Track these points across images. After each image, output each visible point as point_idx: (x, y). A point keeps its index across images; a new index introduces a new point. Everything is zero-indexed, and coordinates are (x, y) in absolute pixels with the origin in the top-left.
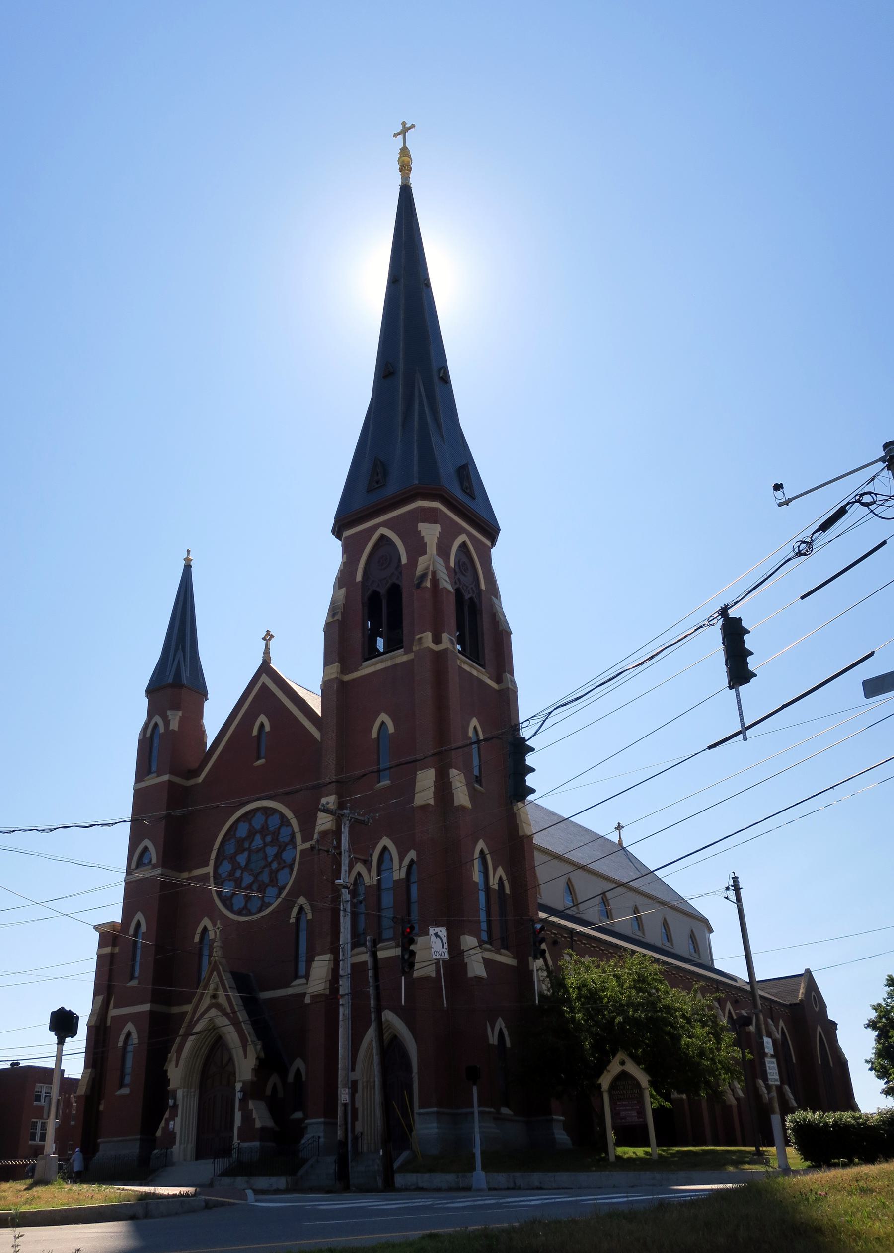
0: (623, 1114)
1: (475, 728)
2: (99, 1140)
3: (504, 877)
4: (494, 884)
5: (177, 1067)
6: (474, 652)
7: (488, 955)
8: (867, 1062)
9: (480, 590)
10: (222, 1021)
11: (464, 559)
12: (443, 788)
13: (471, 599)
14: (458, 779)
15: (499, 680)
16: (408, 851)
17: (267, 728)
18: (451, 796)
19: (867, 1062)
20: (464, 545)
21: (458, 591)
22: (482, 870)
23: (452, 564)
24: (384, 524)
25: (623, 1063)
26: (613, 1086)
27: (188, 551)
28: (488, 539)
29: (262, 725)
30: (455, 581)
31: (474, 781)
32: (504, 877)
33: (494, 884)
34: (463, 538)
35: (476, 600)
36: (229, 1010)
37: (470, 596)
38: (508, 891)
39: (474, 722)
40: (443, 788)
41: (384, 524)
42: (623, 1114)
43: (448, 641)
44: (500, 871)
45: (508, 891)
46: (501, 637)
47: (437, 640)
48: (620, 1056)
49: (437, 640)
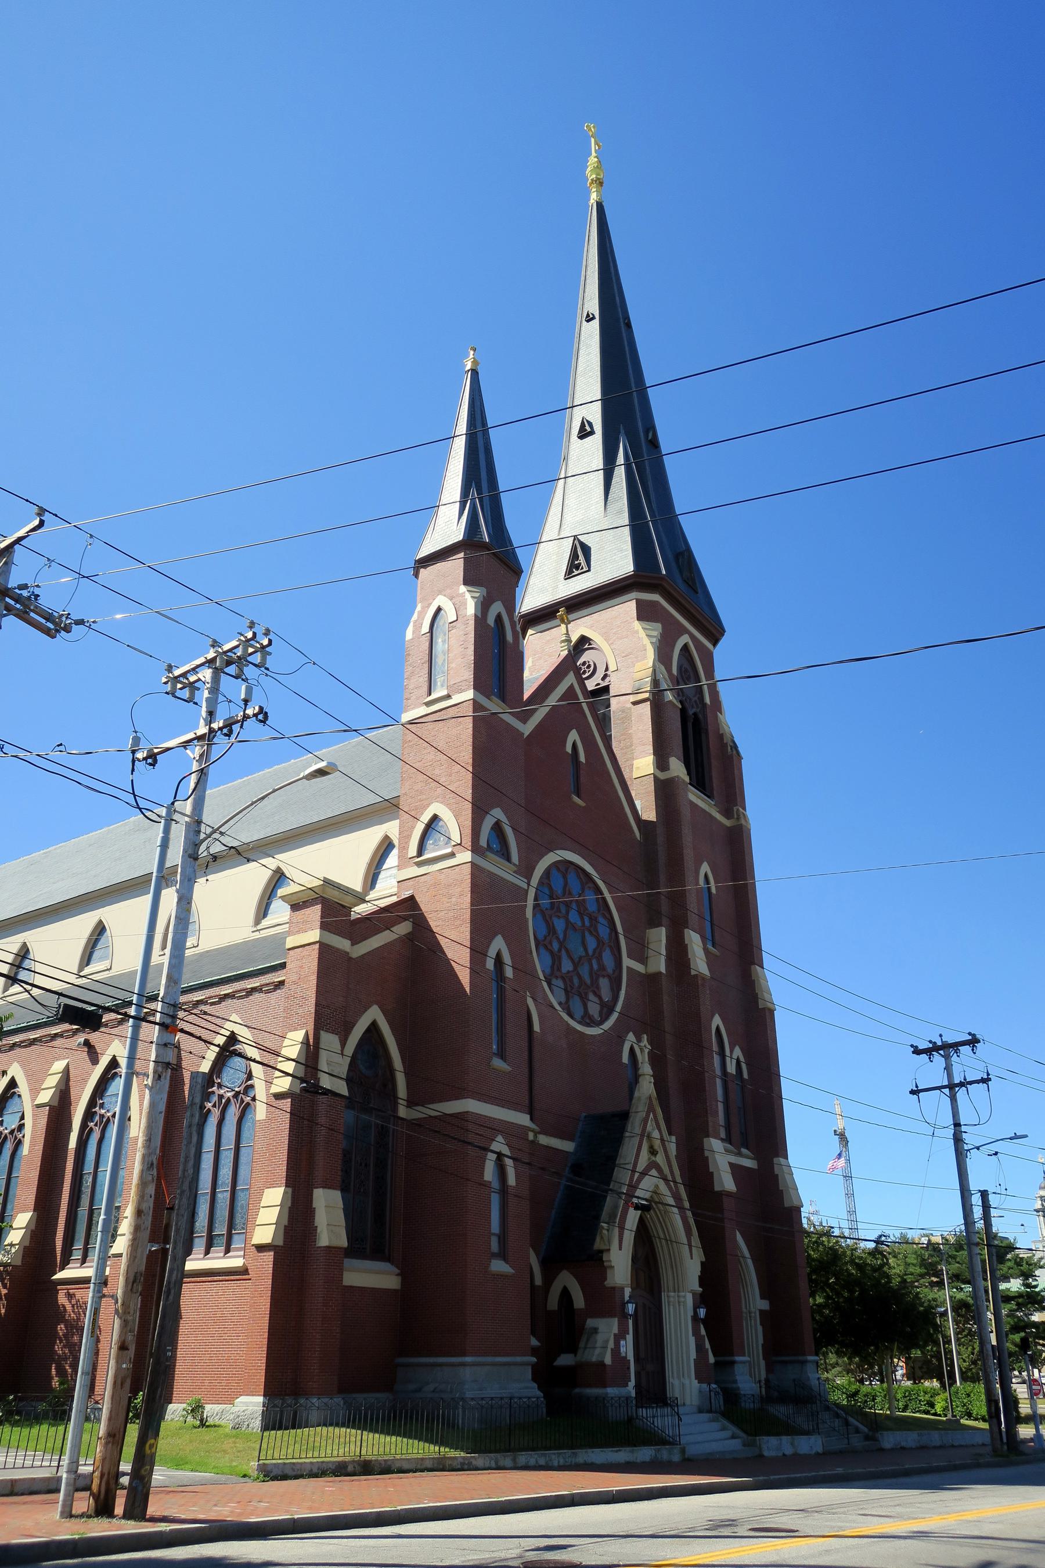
1: (706, 876)
3: (742, 1059)
4: (731, 1068)
5: (620, 1249)
6: (700, 781)
7: (734, 1159)
9: (704, 705)
10: (663, 1189)
11: (686, 665)
13: (695, 714)
14: (694, 941)
15: (728, 813)
20: (685, 648)
21: (683, 711)
22: (121, 1173)
23: (675, 671)
27: (973, 1041)
28: (710, 641)
30: (680, 694)
31: (711, 939)
32: (742, 1059)
33: (731, 1068)
34: (685, 639)
35: (700, 716)
36: (670, 1178)
37: (694, 710)
38: (746, 1076)
39: (705, 868)
44: (738, 1052)
45: (746, 1076)
46: (730, 758)
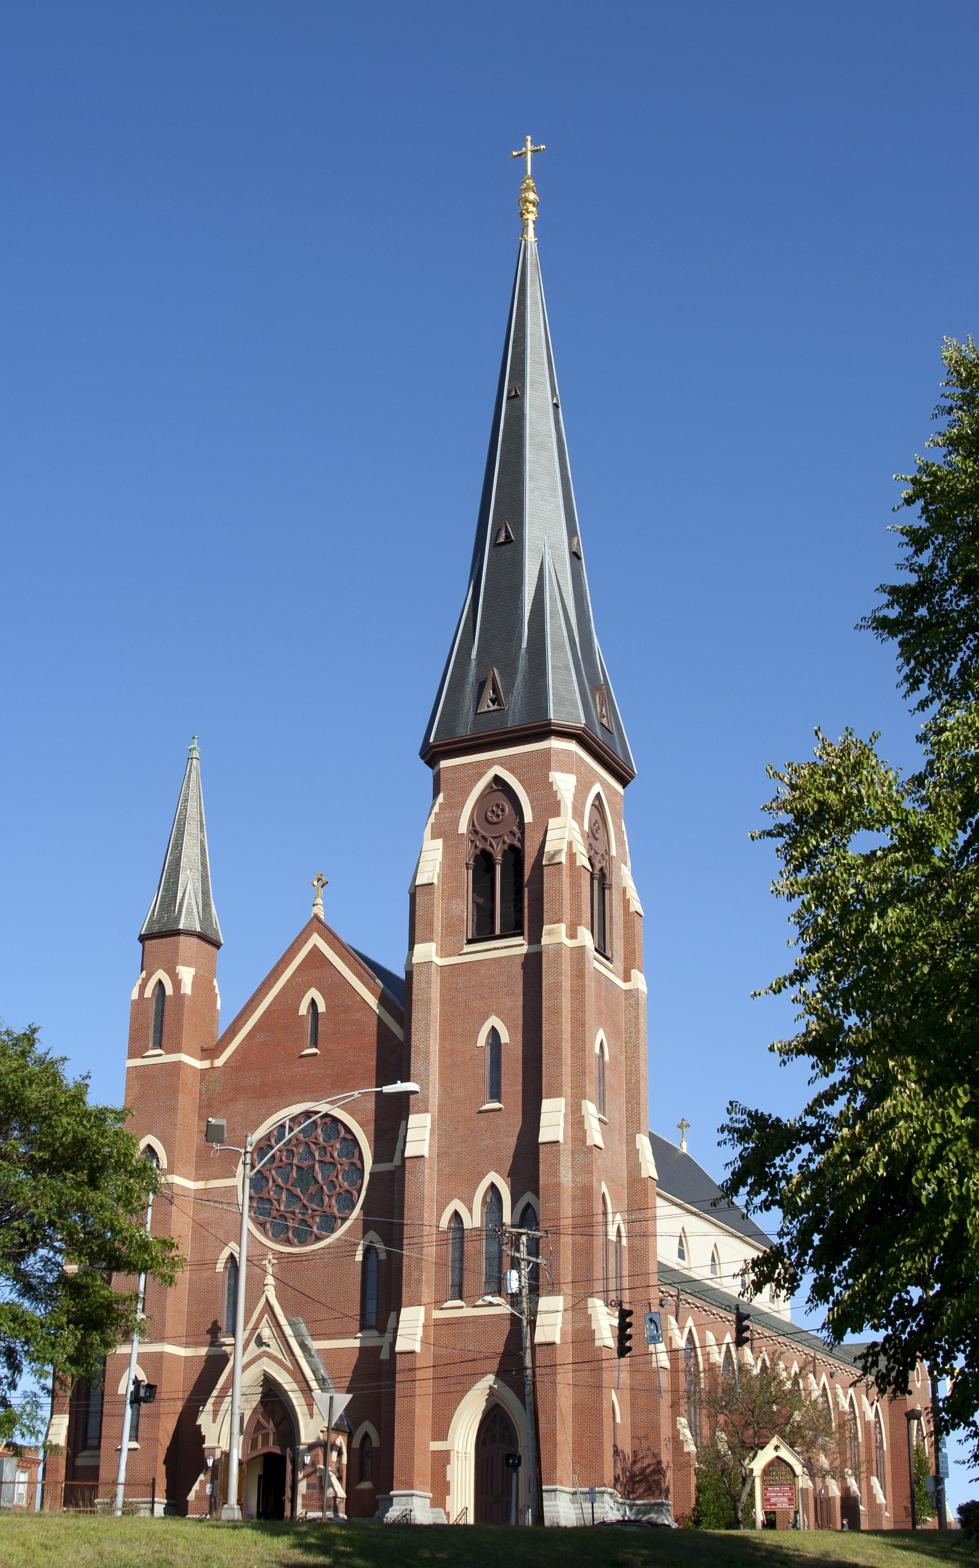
0: (773, 1500)
2: (392, 1493)
8: (789, 1051)
11: (597, 816)
12: (577, 1122)
16: (523, 1193)
17: (322, 1008)
18: (639, 1165)
19: (789, 1051)
23: (586, 828)
24: (502, 762)
25: (777, 1448)
26: (766, 1471)
29: (313, 1003)
40: (577, 1122)
41: (502, 762)
42: (773, 1500)
43: (586, 938)
47: (573, 935)
48: (775, 1441)
49: (573, 935)
